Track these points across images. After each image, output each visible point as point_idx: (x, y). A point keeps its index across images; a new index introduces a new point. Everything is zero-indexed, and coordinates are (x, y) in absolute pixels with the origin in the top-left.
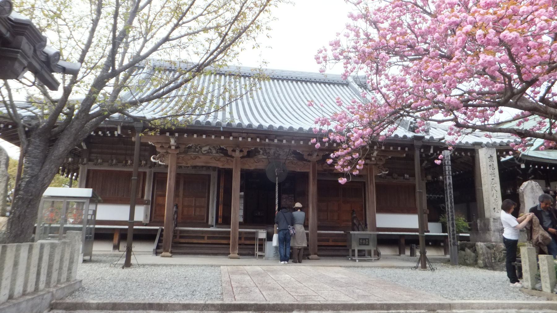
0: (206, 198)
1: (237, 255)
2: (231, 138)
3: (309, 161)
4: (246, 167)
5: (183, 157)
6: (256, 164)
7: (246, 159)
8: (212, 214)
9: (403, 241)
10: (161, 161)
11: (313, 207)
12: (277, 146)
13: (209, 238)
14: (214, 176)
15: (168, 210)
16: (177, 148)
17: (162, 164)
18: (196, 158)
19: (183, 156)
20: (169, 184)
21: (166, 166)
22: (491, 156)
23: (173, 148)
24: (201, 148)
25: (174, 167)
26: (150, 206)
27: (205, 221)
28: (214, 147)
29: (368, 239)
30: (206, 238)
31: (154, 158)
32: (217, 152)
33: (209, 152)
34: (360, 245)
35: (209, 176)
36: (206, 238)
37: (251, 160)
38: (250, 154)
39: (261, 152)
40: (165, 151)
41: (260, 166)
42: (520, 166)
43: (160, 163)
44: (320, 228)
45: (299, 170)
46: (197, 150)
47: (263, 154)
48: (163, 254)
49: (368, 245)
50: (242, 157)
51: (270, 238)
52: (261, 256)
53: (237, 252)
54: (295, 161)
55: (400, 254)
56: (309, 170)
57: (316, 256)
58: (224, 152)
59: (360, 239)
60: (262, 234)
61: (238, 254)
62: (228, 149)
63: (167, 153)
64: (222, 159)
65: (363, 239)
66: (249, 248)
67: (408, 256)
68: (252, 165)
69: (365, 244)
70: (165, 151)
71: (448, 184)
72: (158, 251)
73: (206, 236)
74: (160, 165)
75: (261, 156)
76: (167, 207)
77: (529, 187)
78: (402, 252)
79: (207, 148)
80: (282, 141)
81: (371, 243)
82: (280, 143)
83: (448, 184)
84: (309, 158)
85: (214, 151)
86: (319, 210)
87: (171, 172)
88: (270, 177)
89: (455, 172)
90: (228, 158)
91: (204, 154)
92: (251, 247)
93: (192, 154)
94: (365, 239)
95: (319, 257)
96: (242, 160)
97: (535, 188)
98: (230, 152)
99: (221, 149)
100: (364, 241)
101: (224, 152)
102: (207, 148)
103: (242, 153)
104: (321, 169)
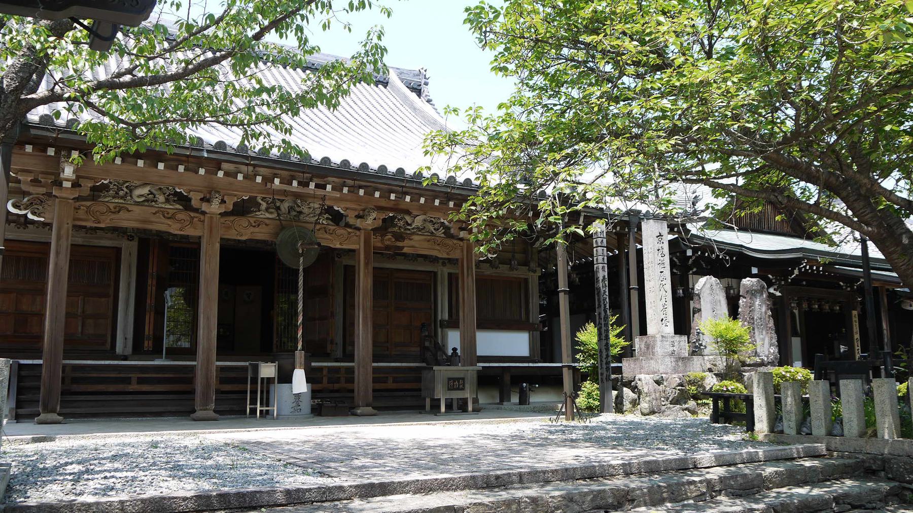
0: (111, 300)
1: (211, 414)
2: (221, 174)
3: (359, 229)
4: (232, 235)
5: (88, 207)
6: (252, 229)
7: (232, 218)
8: (125, 333)
9: (507, 378)
10: (34, 213)
11: (365, 318)
12: (297, 195)
13: (141, 381)
14: (130, 251)
15: (54, 320)
16: (76, 184)
17: (36, 218)
18: (119, 209)
19: (88, 203)
20: (56, 264)
21: (47, 225)
22: (660, 235)
23: (67, 184)
24: (131, 190)
25: (67, 226)
26: (440, 318)
27: (108, 346)
28: (160, 189)
29: (463, 379)
30: (134, 381)
31: (15, 206)
32: (167, 201)
33: (150, 200)
34: (449, 389)
35: (118, 250)
36: (134, 381)
37: (244, 221)
38: (242, 209)
39: (264, 205)
40: (43, 190)
41: (261, 234)
42: (685, 252)
43: (30, 216)
44: (376, 358)
45: (338, 246)
46: (121, 193)
47: (267, 210)
48: (43, 416)
49: (463, 389)
50: (223, 215)
51: (286, 377)
52: (265, 414)
53: (213, 406)
54: (332, 228)
55: (502, 401)
56: (356, 243)
57: (369, 409)
58: (184, 200)
59: (449, 379)
60: (268, 370)
61: (215, 411)
62: (192, 195)
63: (49, 195)
64: (180, 216)
65: (454, 379)
66: (239, 402)
67: (515, 404)
68: (245, 231)
69: (458, 389)
70: (43, 190)
71: (601, 278)
72: (21, 411)
73: (134, 376)
74: (33, 222)
75: (263, 215)
76: (51, 314)
77: (708, 286)
78: (504, 398)
79: (145, 191)
80: (324, 187)
81: (467, 386)
82: (301, 190)
83: (601, 278)
84: (358, 223)
85: (161, 198)
86: (376, 327)
87: (59, 238)
88: (284, 256)
89: (580, 259)
90: (192, 214)
91: (138, 204)
92: (415, 393)
93: (108, 199)
94: (458, 379)
95: (375, 411)
96: (222, 220)
97: (714, 287)
98: (195, 203)
99: (176, 194)
100: (455, 384)
101: (184, 200)
102: (145, 191)
103: (223, 205)
104: (379, 245)
